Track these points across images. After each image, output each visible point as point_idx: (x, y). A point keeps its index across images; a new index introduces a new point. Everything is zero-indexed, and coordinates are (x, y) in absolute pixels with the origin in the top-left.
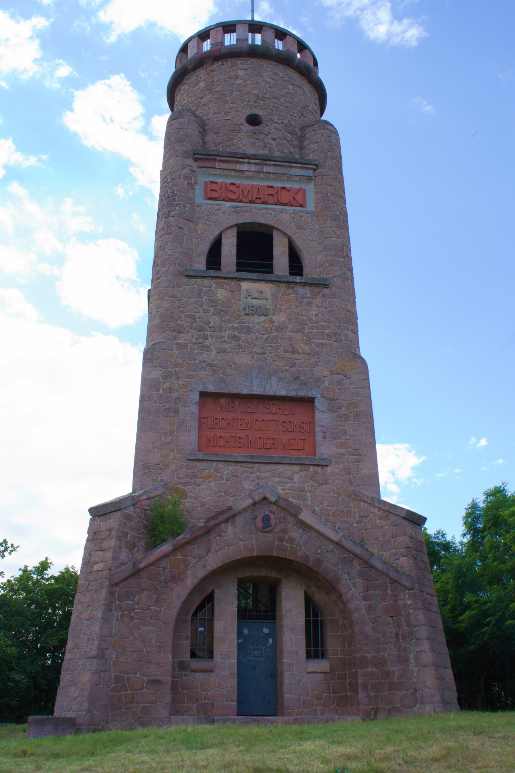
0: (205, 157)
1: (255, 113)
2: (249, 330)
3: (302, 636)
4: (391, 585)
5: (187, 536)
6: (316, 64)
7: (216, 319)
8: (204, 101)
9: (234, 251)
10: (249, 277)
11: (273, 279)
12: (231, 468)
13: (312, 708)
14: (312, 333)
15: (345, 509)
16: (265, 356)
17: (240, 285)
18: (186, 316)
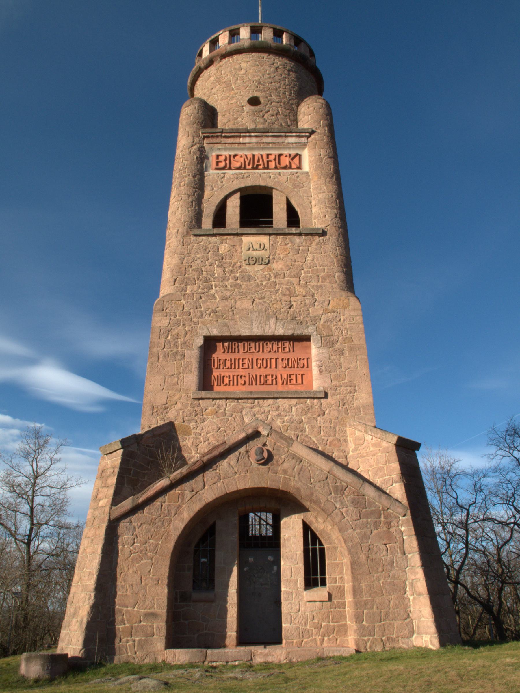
0: (212, 135)
1: (256, 95)
2: (250, 278)
3: (301, 565)
4: (384, 513)
5: (183, 471)
6: (312, 54)
7: (220, 271)
8: (214, 91)
9: (238, 211)
10: (249, 232)
11: (270, 232)
12: (232, 404)
13: (311, 638)
14: (307, 277)
15: (341, 438)
16: (264, 300)
17: (241, 239)
18: (193, 270)
